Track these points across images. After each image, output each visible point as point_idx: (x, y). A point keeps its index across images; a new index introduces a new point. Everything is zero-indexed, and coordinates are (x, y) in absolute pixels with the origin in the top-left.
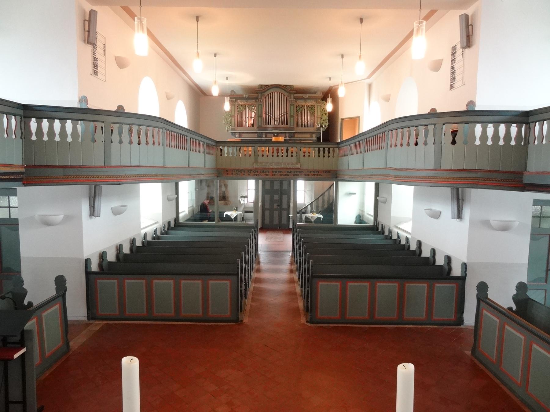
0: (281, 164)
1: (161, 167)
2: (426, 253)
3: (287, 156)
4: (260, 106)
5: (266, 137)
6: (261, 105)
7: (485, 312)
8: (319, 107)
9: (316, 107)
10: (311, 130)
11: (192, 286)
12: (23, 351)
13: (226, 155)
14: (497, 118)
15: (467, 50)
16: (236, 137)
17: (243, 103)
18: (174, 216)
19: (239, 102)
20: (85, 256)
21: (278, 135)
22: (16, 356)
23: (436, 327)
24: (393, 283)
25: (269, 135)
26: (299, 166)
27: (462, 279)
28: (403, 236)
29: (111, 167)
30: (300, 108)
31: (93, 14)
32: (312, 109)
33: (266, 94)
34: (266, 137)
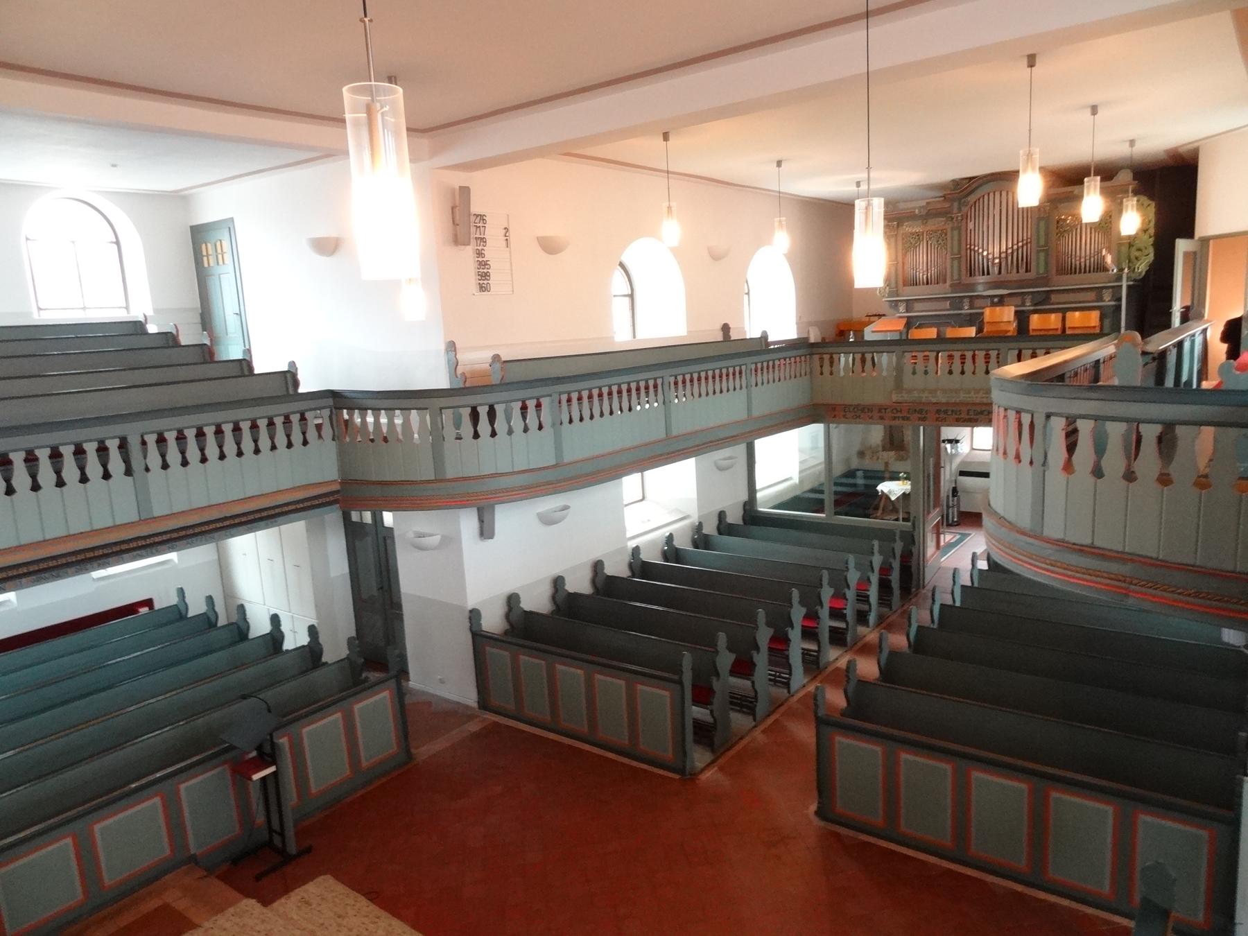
0: (957, 391)
1: (554, 466)
4: (956, 233)
6: (959, 229)
10: (1097, 280)
11: (612, 686)
12: (272, 769)
13: (842, 374)
16: (898, 311)
17: (917, 228)
18: (744, 497)
19: (908, 228)
20: (471, 604)
21: (1001, 301)
22: (256, 777)
29: (449, 480)
31: (465, 191)
33: (972, 198)
34: (971, 308)
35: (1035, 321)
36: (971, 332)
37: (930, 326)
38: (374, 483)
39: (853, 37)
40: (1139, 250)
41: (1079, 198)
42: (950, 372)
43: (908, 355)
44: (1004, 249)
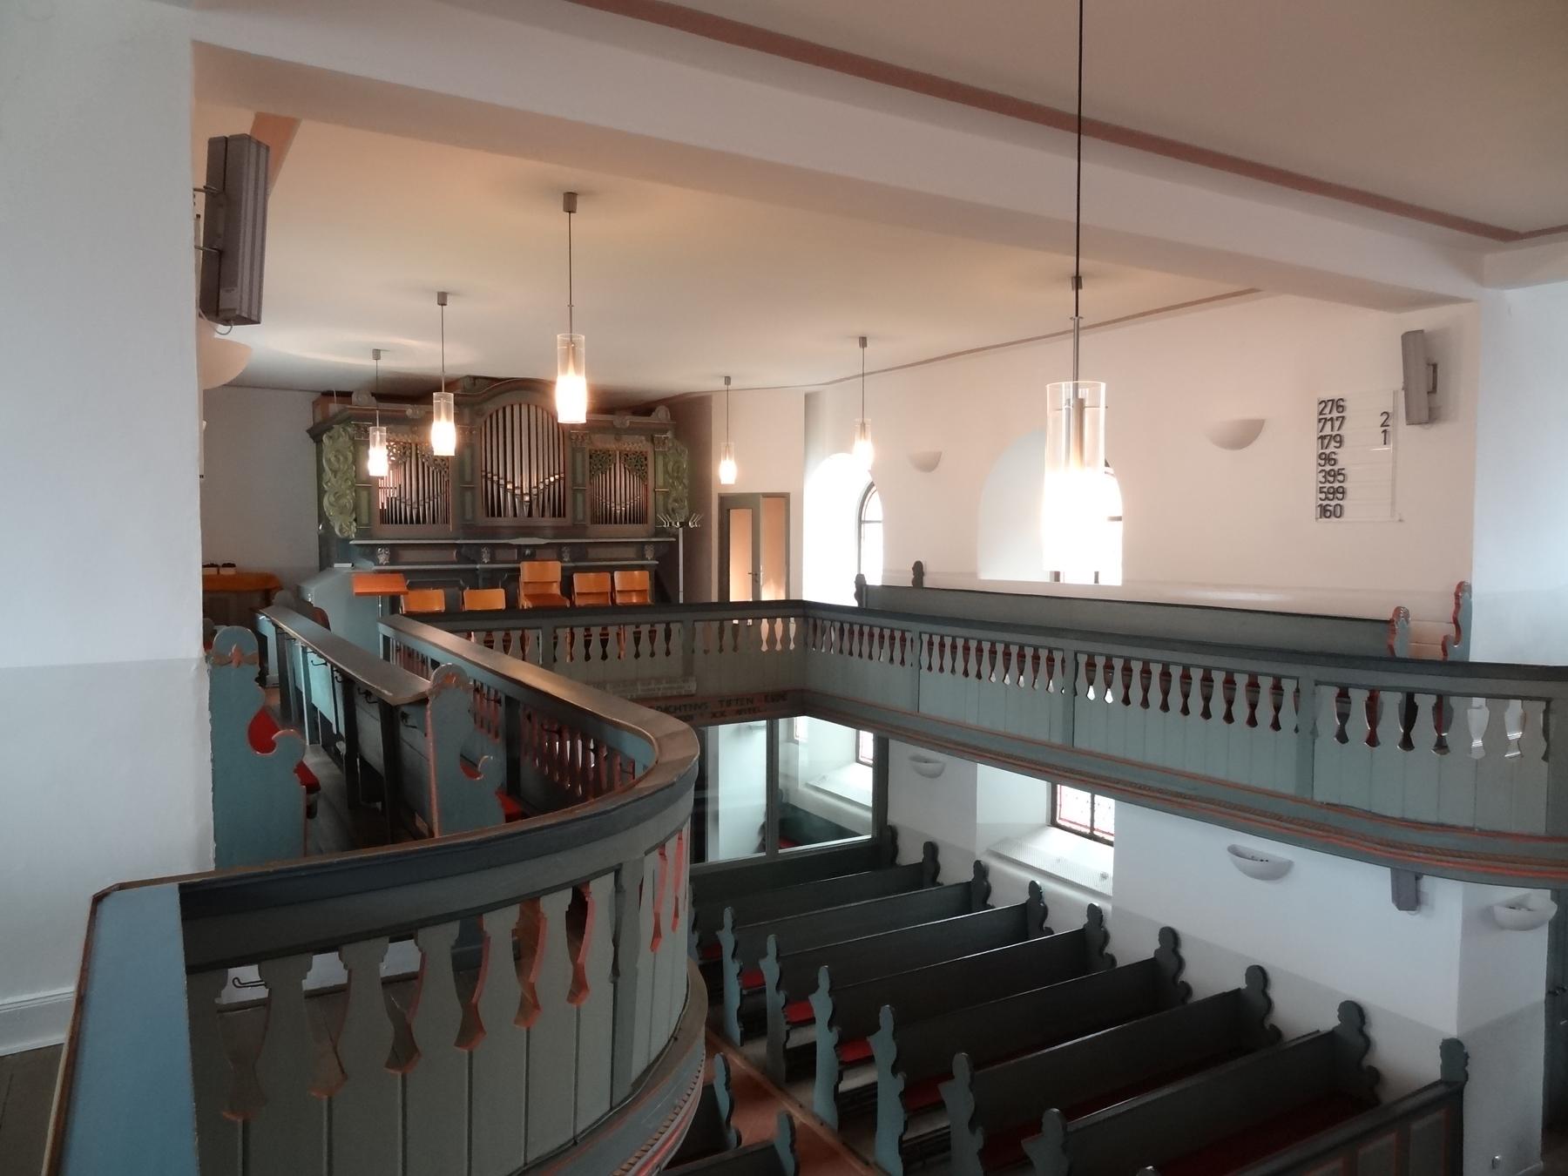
3: (637, 655)
5: (492, 561)
10: (636, 533)
15: (1401, 428)
25: (501, 554)
26: (692, 687)
33: (490, 407)
34: (492, 561)
35: (581, 582)
36: (496, 599)
40: (675, 501)
41: (427, 419)
42: (637, 655)
43: (699, 625)
44: (534, 483)
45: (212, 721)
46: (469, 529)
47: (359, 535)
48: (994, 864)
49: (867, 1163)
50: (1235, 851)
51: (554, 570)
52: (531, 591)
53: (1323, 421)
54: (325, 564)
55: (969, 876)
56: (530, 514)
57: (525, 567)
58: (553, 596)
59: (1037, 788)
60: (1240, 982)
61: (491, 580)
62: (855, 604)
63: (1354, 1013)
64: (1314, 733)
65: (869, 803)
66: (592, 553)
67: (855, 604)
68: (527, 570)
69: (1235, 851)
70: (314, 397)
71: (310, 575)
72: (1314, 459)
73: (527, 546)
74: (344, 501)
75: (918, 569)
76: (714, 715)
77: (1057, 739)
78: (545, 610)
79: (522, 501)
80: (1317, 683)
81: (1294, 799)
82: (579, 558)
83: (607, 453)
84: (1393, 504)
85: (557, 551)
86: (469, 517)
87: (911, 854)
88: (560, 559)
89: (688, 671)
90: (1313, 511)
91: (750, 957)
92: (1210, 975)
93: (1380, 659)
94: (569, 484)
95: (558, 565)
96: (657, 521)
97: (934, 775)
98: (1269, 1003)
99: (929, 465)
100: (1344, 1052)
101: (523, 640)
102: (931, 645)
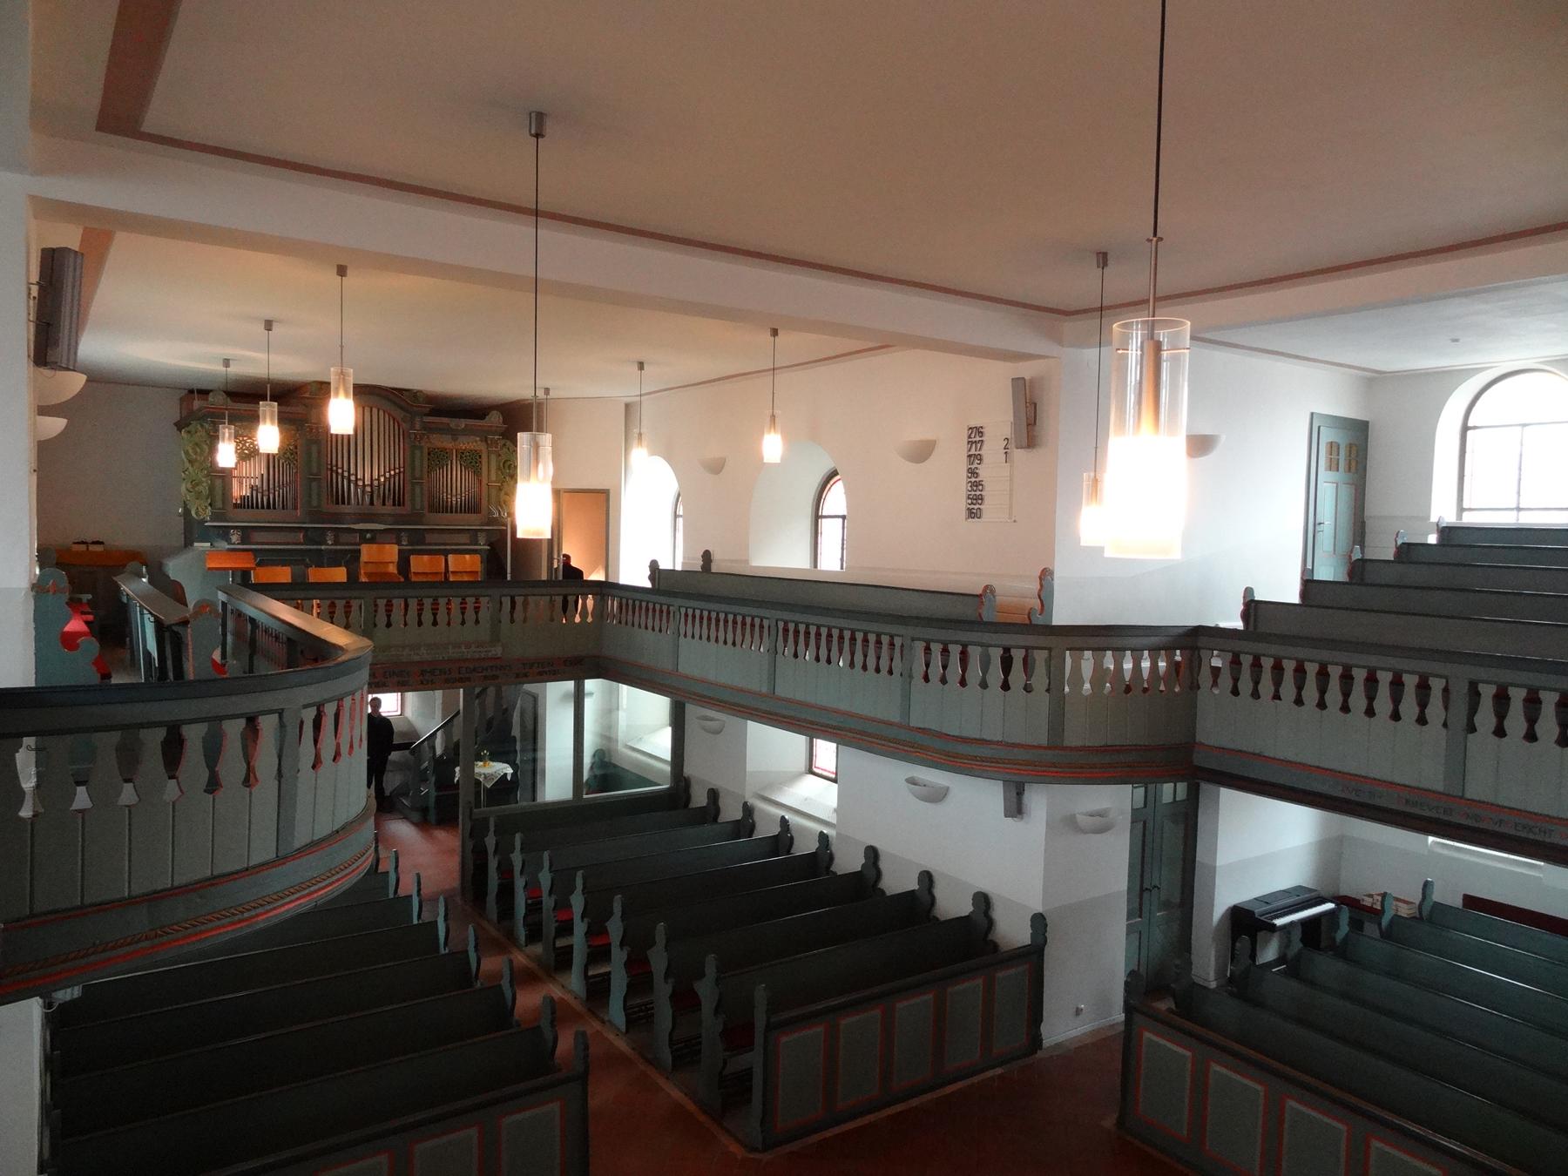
2: (898, 880)
3: (463, 623)
5: (336, 543)
7: (1147, 1035)
8: (493, 457)
9: (484, 456)
10: (471, 521)
14: (1154, 640)
15: (1019, 455)
23: (999, 1071)
24: (1335, 1118)
25: (344, 537)
26: (497, 651)
27: (1033, 956)
28: (804, 829)
30: (438, 458)
32: (472, 462)
35: (419, 564)
36: (339, 574)
37: (335, 563)
38: (132, 901)
39: (519, 231)
41: (254, 419)
45: (36, 629)
46: (316, 515)
47: (214, 517)
48: (760, 805)
49: (603, 1022)
50: (912, 781)
51: (391, 552)
52: (370, 569)
53: (970, 443)
54: (188, 543)
55: (738, 815)
56: (372, 503)
57: (364, 548)
58: (390, 574)
59: (798, 741)
60: (913, 885)
61: (334, 560)
62: (648, 585)
63: (983, 901)
64: (911, 677)
65: (668, 758)
66: (429, 538)
67: (648, 585)
68: (367, 552)
69: (912, 781)
70: (184, 393)
71: (174, 552)
72: (965, 474)
73: (367, 531)
74: (200, 488)
75: (707, 556)
76: (517, 676)
77: (764, 690)
78: (380, 583)
79: (363, 492)
80: (913, 640)
81: (900, 726)
82: (417, 542)
83: (443, 450)
84: (1011, 507)
85: (395, 536)
86: (315, 503)
87: (699, 799)
88: (399, 543)
89: (495, 638)
90: (964, 513)
91: (531, 868)
92: (952, 904)
93: (972, 622)
94: (408, 478)
95: (396, 548)
96: (490, 512)
97: (718, 732)
98: (933, 899)
99: (716, 467)
100: (976, 928)
101: (348, 606)
102: (717, 621)
